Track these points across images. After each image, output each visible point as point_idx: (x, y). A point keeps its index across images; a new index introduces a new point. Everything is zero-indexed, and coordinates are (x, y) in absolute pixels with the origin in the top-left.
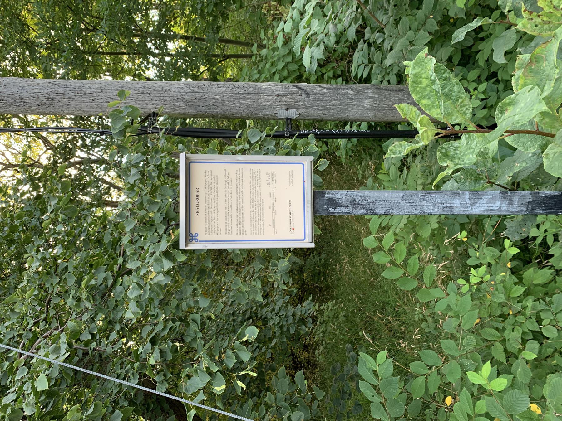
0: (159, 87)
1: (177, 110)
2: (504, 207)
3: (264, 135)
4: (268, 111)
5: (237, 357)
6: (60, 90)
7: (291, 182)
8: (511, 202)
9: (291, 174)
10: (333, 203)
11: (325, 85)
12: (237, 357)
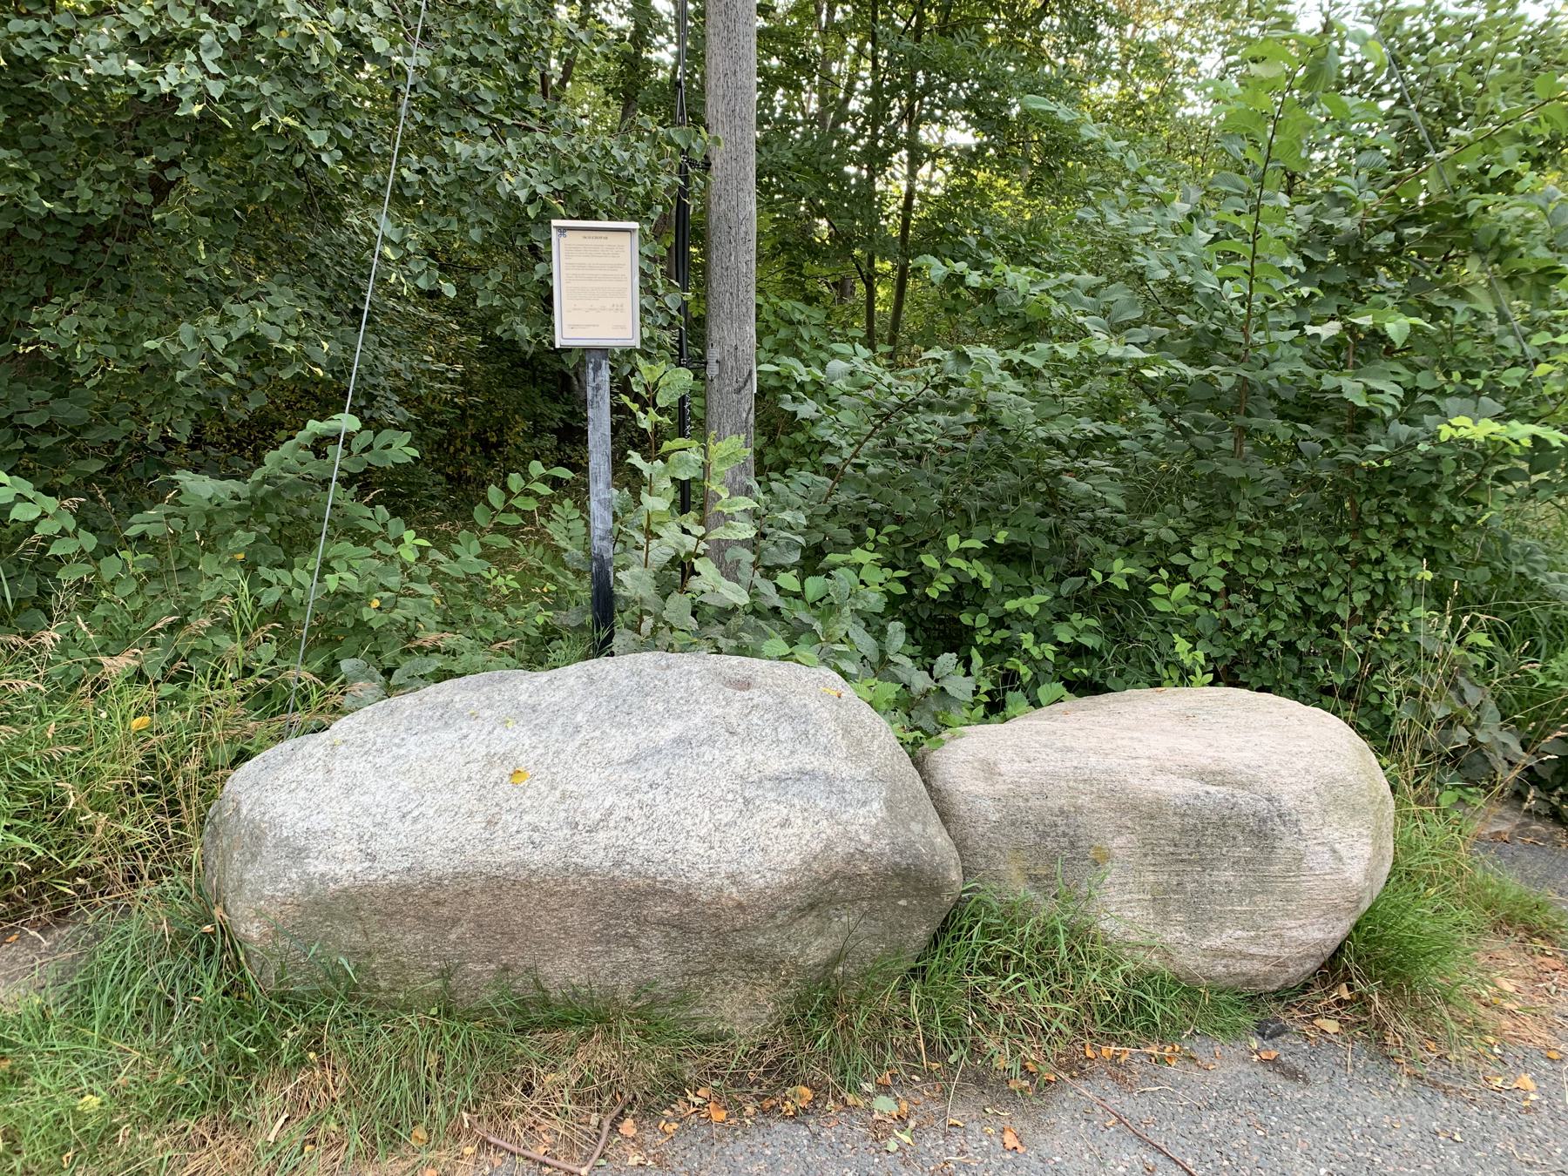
0: (746, 175)
1: (714, 200)
2: (598, 532)
3: (675, 313)
4: (715, 334)
5: (421, 273)
6: (740, 27)
7: (616, 327)
8: (602, 539)
9: (623, 327)
10: (597, 368)
11: (752, 416)
12: (421, 273)
